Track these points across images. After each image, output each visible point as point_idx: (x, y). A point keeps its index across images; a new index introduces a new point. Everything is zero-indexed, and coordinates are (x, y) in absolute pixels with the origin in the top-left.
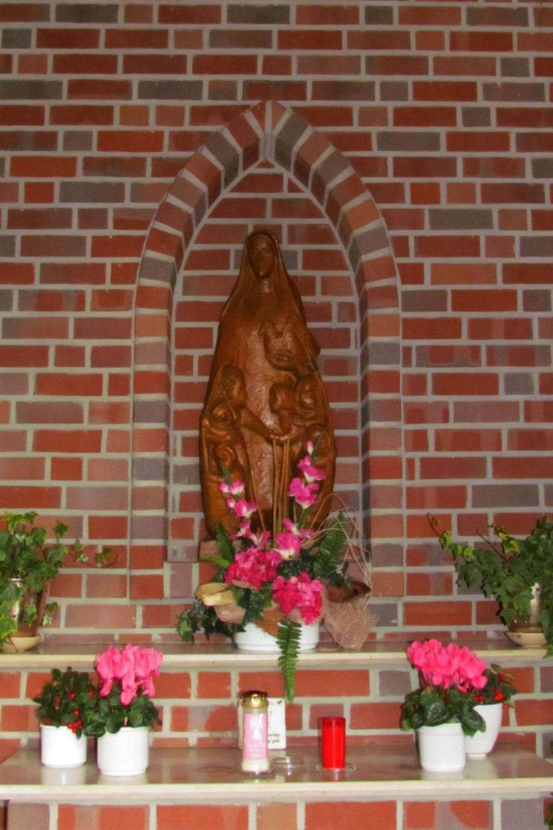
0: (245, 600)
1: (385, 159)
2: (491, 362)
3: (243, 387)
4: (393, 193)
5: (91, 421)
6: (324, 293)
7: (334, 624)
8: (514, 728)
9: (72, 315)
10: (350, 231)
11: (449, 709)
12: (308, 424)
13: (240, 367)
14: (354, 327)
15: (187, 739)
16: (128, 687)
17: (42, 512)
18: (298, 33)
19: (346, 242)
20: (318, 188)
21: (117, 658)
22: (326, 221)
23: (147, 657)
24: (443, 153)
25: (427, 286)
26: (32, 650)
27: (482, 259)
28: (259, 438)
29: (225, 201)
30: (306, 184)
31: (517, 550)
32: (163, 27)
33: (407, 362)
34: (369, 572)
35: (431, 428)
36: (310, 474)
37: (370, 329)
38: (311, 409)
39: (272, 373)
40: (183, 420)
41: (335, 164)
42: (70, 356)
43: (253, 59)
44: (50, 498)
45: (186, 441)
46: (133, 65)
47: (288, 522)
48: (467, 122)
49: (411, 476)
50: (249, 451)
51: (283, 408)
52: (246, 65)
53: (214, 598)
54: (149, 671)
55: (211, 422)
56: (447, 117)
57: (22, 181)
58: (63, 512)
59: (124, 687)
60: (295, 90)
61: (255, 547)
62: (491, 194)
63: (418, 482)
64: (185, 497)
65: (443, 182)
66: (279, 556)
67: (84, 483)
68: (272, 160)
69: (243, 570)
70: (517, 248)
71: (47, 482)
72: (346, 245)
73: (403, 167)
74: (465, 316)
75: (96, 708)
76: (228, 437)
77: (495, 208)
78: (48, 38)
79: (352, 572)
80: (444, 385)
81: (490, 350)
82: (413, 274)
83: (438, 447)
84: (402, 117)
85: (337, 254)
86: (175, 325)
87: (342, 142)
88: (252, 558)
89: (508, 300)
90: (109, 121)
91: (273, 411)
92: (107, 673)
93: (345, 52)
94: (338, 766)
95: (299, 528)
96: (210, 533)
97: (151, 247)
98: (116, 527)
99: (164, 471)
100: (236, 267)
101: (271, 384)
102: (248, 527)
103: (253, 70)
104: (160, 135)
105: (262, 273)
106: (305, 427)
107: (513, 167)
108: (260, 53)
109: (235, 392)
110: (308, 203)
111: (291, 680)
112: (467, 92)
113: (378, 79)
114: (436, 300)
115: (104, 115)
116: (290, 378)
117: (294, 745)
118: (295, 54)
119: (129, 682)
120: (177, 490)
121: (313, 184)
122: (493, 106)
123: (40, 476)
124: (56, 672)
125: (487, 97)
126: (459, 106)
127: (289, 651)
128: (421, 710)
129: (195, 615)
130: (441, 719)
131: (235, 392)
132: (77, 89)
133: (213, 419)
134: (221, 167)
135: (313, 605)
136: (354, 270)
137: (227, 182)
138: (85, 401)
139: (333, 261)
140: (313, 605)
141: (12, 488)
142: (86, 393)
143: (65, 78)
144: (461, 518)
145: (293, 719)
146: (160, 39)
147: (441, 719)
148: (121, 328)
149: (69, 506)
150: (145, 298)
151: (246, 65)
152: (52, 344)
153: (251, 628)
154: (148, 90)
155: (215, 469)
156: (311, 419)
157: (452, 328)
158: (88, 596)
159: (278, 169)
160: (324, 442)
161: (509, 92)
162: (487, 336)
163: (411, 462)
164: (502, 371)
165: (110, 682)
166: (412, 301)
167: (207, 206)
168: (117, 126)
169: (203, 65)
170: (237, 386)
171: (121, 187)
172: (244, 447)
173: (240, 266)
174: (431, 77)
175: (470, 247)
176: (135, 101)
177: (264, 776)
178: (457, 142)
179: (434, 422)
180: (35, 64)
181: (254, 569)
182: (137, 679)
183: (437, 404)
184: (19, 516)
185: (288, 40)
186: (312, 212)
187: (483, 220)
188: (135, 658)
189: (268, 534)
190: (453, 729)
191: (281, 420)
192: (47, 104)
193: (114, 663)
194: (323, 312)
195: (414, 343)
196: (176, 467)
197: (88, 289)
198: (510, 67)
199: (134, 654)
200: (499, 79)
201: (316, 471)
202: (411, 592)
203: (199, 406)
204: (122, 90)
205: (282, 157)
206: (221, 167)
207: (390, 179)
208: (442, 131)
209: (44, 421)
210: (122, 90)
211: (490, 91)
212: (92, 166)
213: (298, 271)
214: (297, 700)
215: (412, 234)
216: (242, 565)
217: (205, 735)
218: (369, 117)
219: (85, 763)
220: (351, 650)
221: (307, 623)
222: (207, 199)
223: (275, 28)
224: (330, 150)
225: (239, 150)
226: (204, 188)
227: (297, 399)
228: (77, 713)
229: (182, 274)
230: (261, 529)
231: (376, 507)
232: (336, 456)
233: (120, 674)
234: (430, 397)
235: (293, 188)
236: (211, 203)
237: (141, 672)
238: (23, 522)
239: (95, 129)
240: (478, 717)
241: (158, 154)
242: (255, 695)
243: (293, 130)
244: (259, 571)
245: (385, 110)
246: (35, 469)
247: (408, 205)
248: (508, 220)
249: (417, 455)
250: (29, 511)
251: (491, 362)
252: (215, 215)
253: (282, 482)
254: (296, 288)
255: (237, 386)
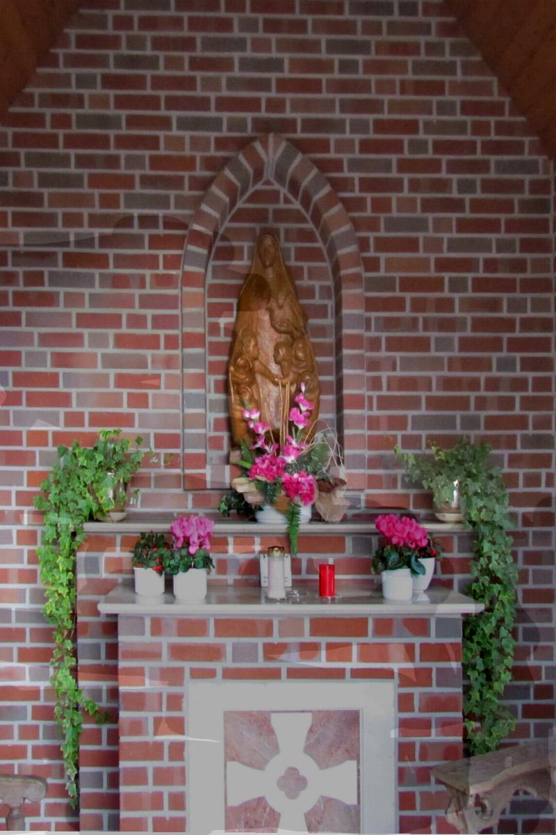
0: (263, 488)
1: (353, 179)
2: (426, 329)
3: (256, 345)
4: (358, 204)
5: (153, 367)
6: (310, 278)
7: (322, 509)
8: (441, 576)
9: (137, 292)
10: (329, 232)
11: (403, 560)
12: (301, 371)
13: (254, 330)
14: (331, 303)
15: (226, 580)
16: (194, 543)
17: (125, 430)
18: (291, 80)
19: (325, 241)
20: (306, 201)
21: (185, 524)
22: (310, 225)
23: (205, 524)
24: (394, 174)
25: (382, 273)
26: (121, 521)
27: (421, 254)
28: (267, 381)
29: (240, 210)
30: (296, 199)
31: (443, 458)
32: (192, 73)
33: (368, 328)
34: (342, 472)
35: (384, 375)
36: (303, 405)
37: (344, 304)
38: (303, 361)
39: (276, 335)
40: (213, 368)
41: (316, 183)
42: (137, 321)
43: (258, 100)
44: (127, 420)
45: (216, 382)
46: (173, 103)
47: (289, 437)
48: (411, 151)
49: (371, 408)
50: (260, 390)
51: (284, 360)
52: (253, 105)
53: (243, 486)
54: (206, 533)
55: (235, 369)
56: (396, 147)
57: (96, 192)
58: (136, 430)
59: (191, 542)
60: (289, 125)
61: (268, 454)
62: (428, 206)
63: (376, 412)
64: (217, 421)
65: (394, 196)
66: (284, 461)
67: (150, 410)
68: (272, 180)
69: (261, 469)
70: (445, 246)
71: (125, 409)
72: (325, 244)
73: (367, 185)
74: (408, 296)
75: (172, 557)
76: (247, 379)
77: (430, 216)
78: (109, 81)
79: (332, 473)
80: (394, 345)
81: (426, 321)
82: (372, 265)
83: (389, 388)
84: (366, 146)
85: (318, 250)
86: (208, 300)
87: (323, 166)
88: (267, 461)
89: (437, 285)
90: (157, 147)
91: (277, 362)
92: (179, 533)
93: (324, 95)
94: (330, 595)
95: (297, 442)
96: (234, 445)
97: (191, 242)
98: (172, 441)
99: (202, 401)
100: (248, 259)
101: (275, 343)
102: (263, 441)
103: (258, 109)
104: (193, 159)
105: (267, 263)
106: (299, 373)
107: (443, 185)
108: (263, 95)
109: (251, 348)
110: (298, 211)
111: (295, 542)
112: (411, 127)
113: (348, 117)
114: (388, 284)
115: (153, 143)
116: (288, 338)
117: (297, 583)
118: (288, 96)
119: (194, 539)
120: (212, 416)
121: (301, 198)
122: (430, 138)
123: (120, 405)
124: (143, 534)
125: (427, 131)
126: (406, 138)
127: (293, 523)
128: (384, 560)
129: (471, 455)
130: (398, 566)
131: (251, 348)
132: (133, 122)
133: (237, 367)
134: (238, 184)
135: (309, 493)
136: (331, 262)
137: (243, 193)
138: (148, 353)
139: (314, 255)
140: (309, 493)
141: (101, 413)
142: (149, 347)
143: (124, 113)
144: (404, 437)
145: (296, 569)
146: (190, 83)
147: (398, 566)
148: (171, 302)
149: (140, 426)
150: (189, 279)
151: (253, 105)
152: (124, 312)
153: (267, 508)
154: (184, 124)
155: (238, 402)
156: (303, 368)
157: (399, 304)
158: (155, 487)
159: (276, 186)
160: (312, 383)
161: (443, 127)
162: (424, 310)
163: (370, 398)
164: (433, 335)
165: (182, 539)
166: (373, 284)
167: (228, 212)
168: (162, 152)
169: (223, 104)
170: (253, 343)
171: (167, 197)
172: (258, 388)
173: (251, 258)
174: (385, 116)
175: (412, 245)
176: (175, 132)
177: (282, 601)
178: (404, 166)
179: (386, 370)
180: (101, 102)
181: (268, 469)
182: (199, 537)
183: (388, 358)
184: (110, 432)
185: (283, 85)
186: (301, 219)
187: (420, 225)
188: (197, 524)
189: (277, 446)
190: (405, 571)
191: (282, 368)
192: (112, 133)
193: (184, 527)
194: (310, 293)
195: (373, 315)
196: (210, 400)
197: (148, 273)
198: (444, 108)
199: (196, 521)
200: (434, 117)
201: (308, 403)
202: (370, 487)
203: (225, 358)
204: (165, 123)
205: (280, 177)
206: (238, 184)
207: (357, 194)
208: (394, 158)
209: (122, 367)
210: (165, 123)
211: (429, 127)
212: (147, 181)
213: (293, 263)
214: (299, 556)
215: (371, 235)
216: (260, 466)
217: (238, 577)
218: (344, 146)
219: (164, 593)
220: (332, 523)
221: (305, 504)
222: (228, 209)
223: (273, 76)
224: (315, 171)
225: (251, 171)
226: (227, 199)
227: (293, 353)
228: (158, 560)
229: (212, 263)
230: (272, 443)
231: (347, 428)
232: (320, 394)
233: (188, 534)
234: (383, 353)
235: (287, 201)
236: (231, 210)
237: (202, 534)
238: (112, 436)
239: (147, 153)
240: (421, 566)
241: (193, 173)
242: (276, 549)
243: (287, 158)
244: (272, 470)
245: (352, 141)
246: (116, 399)
247: (368, 213)
248: (440, 225)
249: (375, 394)
250: (116, 429)
251: (426, 329)
252: (233, 220)
253: (281, 409)
254: (294, 274)
255: (253, 343)
